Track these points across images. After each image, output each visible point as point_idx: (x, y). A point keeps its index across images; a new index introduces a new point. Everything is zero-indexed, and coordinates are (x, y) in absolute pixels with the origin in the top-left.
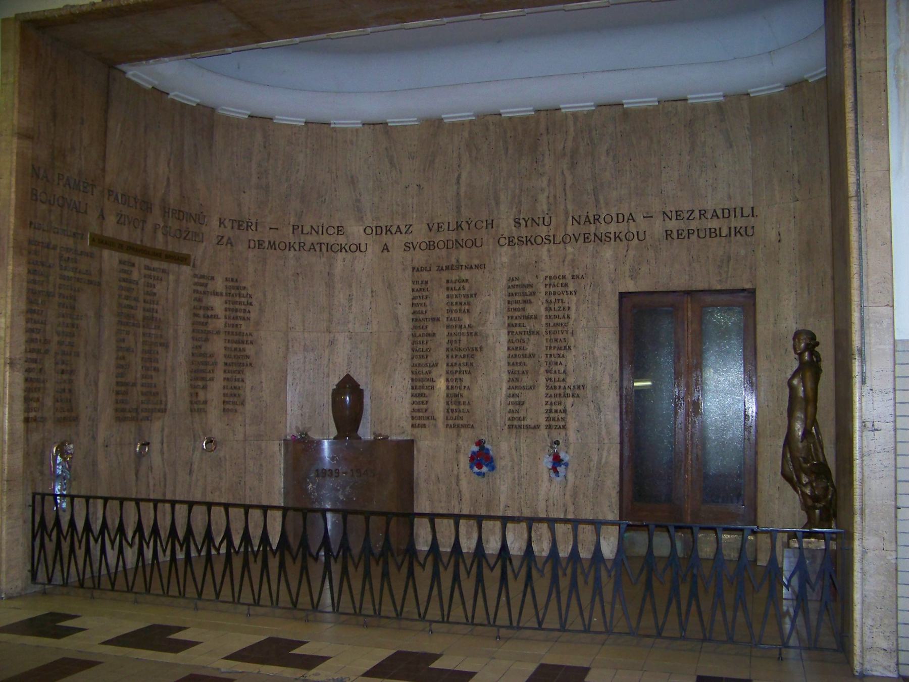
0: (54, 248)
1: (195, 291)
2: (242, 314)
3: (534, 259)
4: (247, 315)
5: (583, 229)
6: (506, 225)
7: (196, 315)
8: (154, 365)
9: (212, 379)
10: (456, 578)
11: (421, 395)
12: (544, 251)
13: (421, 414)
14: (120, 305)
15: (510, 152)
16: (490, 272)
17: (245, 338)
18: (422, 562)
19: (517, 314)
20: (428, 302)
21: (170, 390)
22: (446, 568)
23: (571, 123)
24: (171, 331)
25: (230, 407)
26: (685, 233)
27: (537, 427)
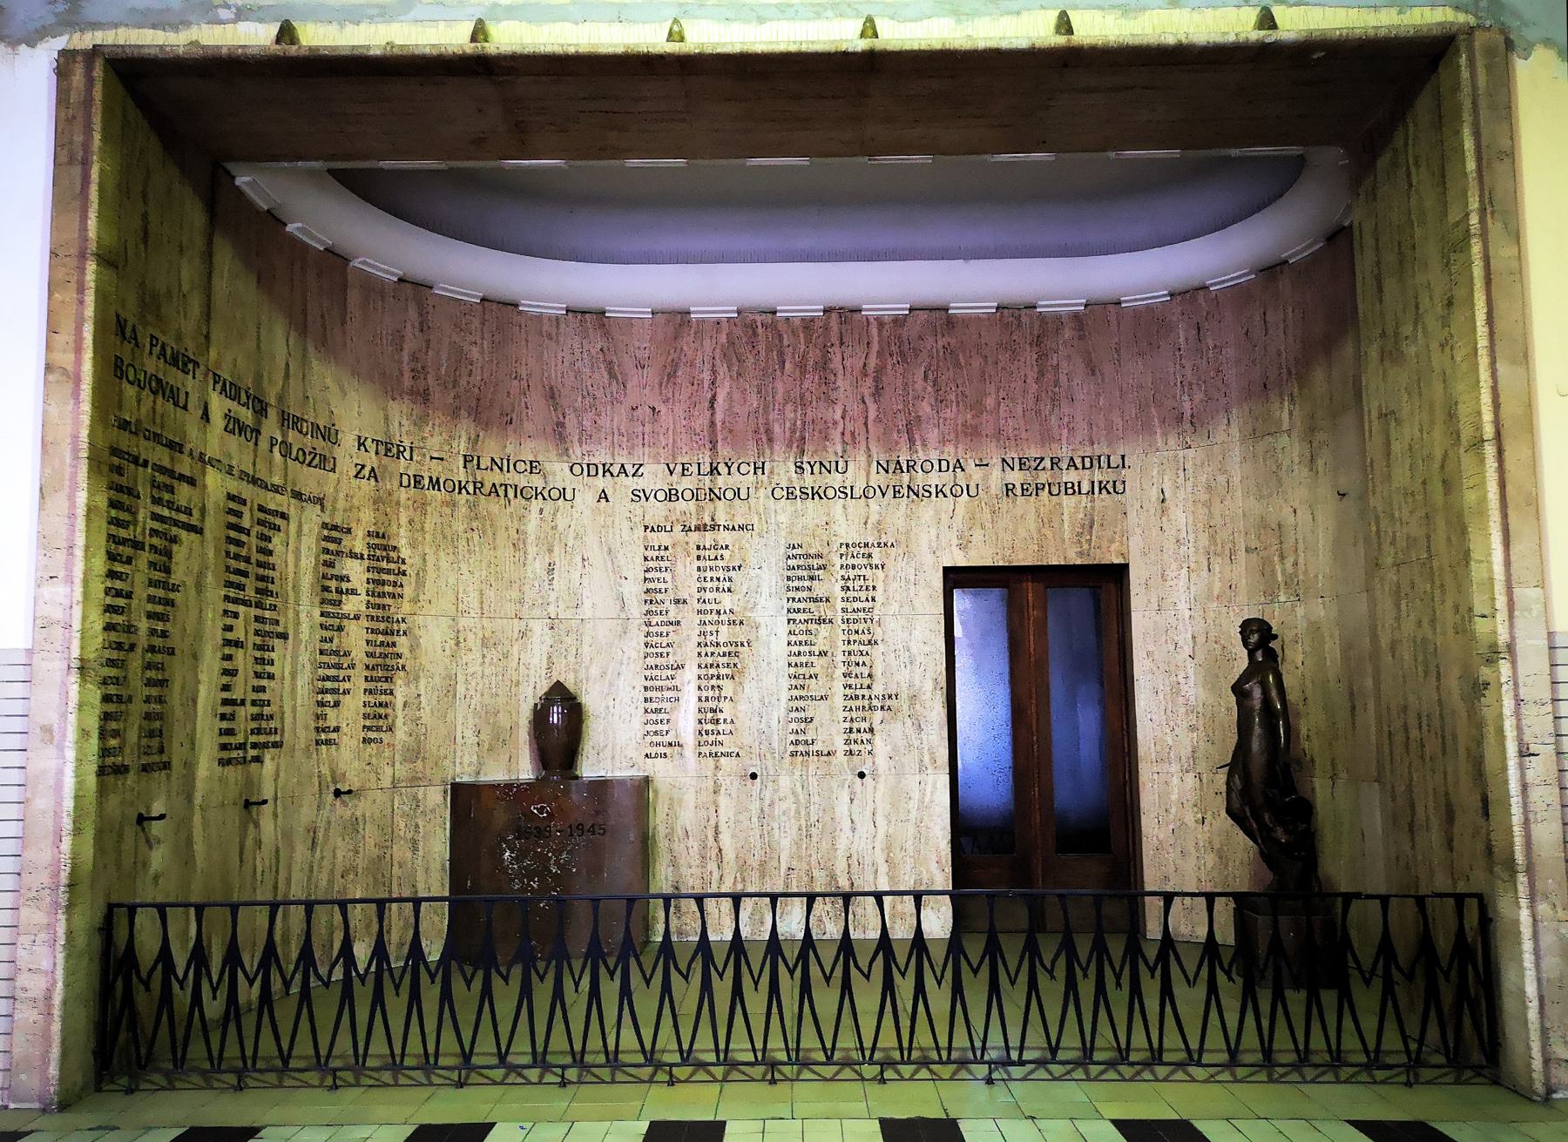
3: (825, 519)
15: (787, 365)
18: (866, 970)
22: (721, 976)
23: (874, 331)
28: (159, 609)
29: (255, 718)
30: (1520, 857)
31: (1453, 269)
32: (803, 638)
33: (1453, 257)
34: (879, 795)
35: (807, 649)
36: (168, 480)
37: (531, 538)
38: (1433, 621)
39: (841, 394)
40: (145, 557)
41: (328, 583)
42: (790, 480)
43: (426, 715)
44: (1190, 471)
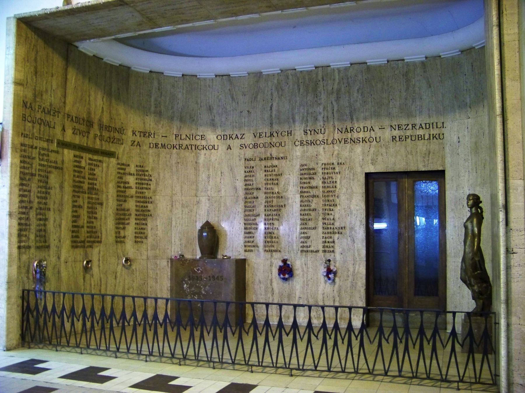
0: (36, 148)
1: (119, 173)
2: (146, 186)
3: (316, 153)
4: (149, 186)
8: (94, 215)
9: (128, 224)
11: (250, 233)
12: (321, 149)
13: (250, 244)
14: (74, 181)
16: (290, 161)
17: (148, 200)
20: (254, 178)
25: (139, 240)
26: (404, 138)
27: (317, 251)
28: (44, 195)
29: (88, 232)
32: (306, 203)
35: (308, 208)
37: (201, 165)
39: (323, 101)
41: (120, 185)
42: (302, 138)
43: (160, 233)
44: (470, 128)
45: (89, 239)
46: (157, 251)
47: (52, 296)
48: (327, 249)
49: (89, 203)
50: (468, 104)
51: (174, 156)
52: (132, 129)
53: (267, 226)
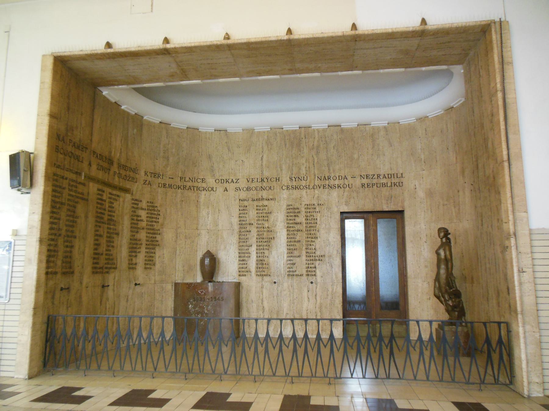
0: (66, 179)
1: (133, 207)
2: (155, 220)
3: (299, 196)
4: (157, 220)
5: (323, 183)
6: (285, 180)
7: (133, 219)
8: (112, 244)
9: (139, 252)
10: (306, 352)
11: (243, 260)
12: (304, 192)
13: (243, 270)
14: (97, 212)
16: (278, 202)
17: (156, 232)
18: (287, 345)
19: (291, 222)
20: (247, 216)
21: (118, 257)
24: (120, 227)
25: (148, 266)
26: (371, 185)
27: (302, 275)
28: (71, 224)
29: (106, 259)
30: (519, 309)
31: (493, 102)
32: (292, 236)
33: (493, 98)
34: (318, 289)
35: (293, 240)
36: (75, 184)
37: (202, 204)
38: (492, 226)
40: (65, 207)
45: (106, 266)
46: (164, 276)
47: (139, 321)
48: (309, 273)
49: (108, 232)
50: (423, 160)
51: (179, 195)
52: (144, 170)
53: (258, 255)
